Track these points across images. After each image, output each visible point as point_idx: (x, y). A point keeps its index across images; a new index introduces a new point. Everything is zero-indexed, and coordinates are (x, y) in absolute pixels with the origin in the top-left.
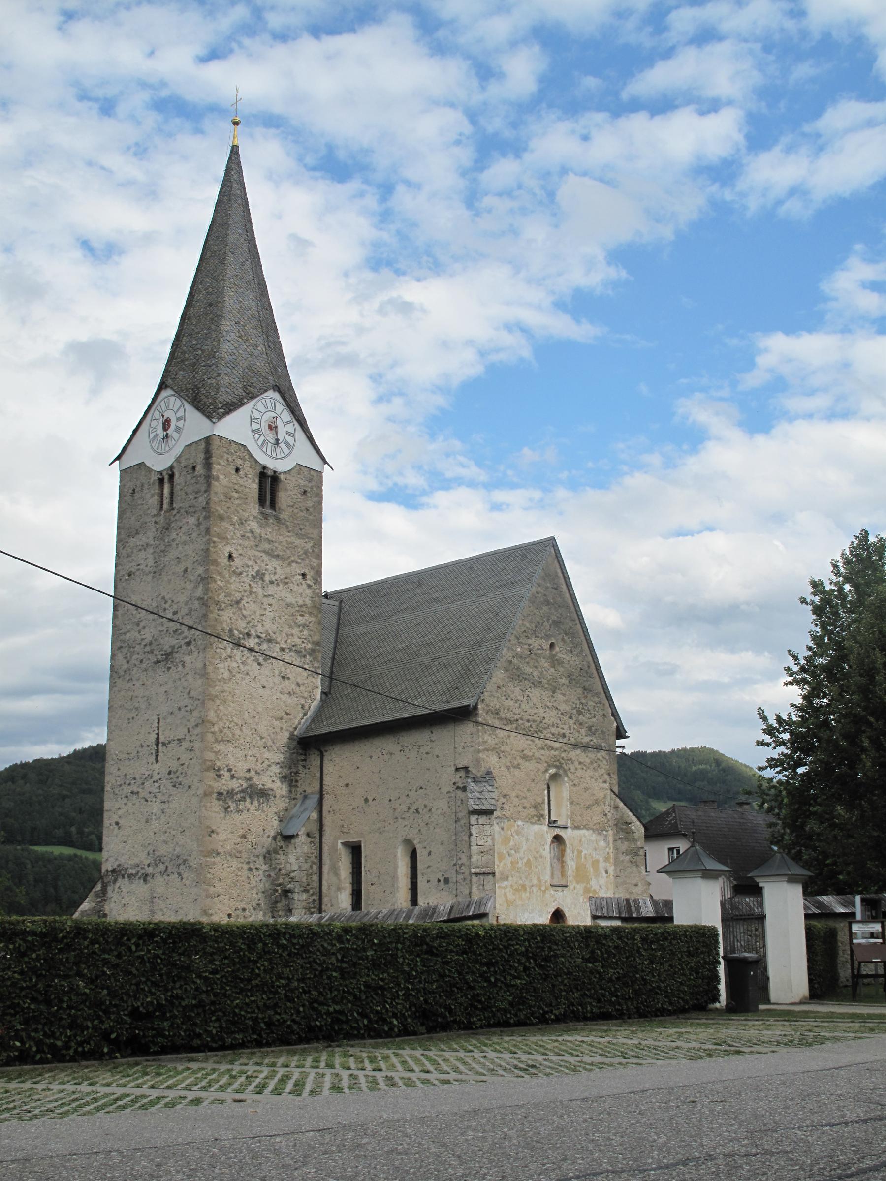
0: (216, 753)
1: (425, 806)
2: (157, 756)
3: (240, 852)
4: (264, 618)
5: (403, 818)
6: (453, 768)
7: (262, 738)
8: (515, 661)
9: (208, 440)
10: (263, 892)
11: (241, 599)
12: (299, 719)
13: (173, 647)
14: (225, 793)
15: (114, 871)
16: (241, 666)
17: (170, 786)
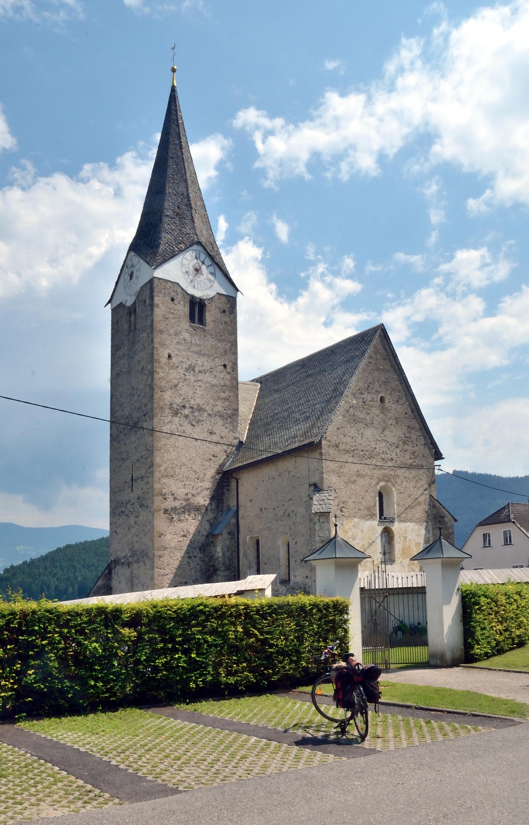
1: (293, 511)
2: (132, 488)
4: (195, 395)
6: (308, 485)
9: (151, 282)
11: (178, 384)
13: (138, 418)
15: (115, 561)
17: (138, 507)
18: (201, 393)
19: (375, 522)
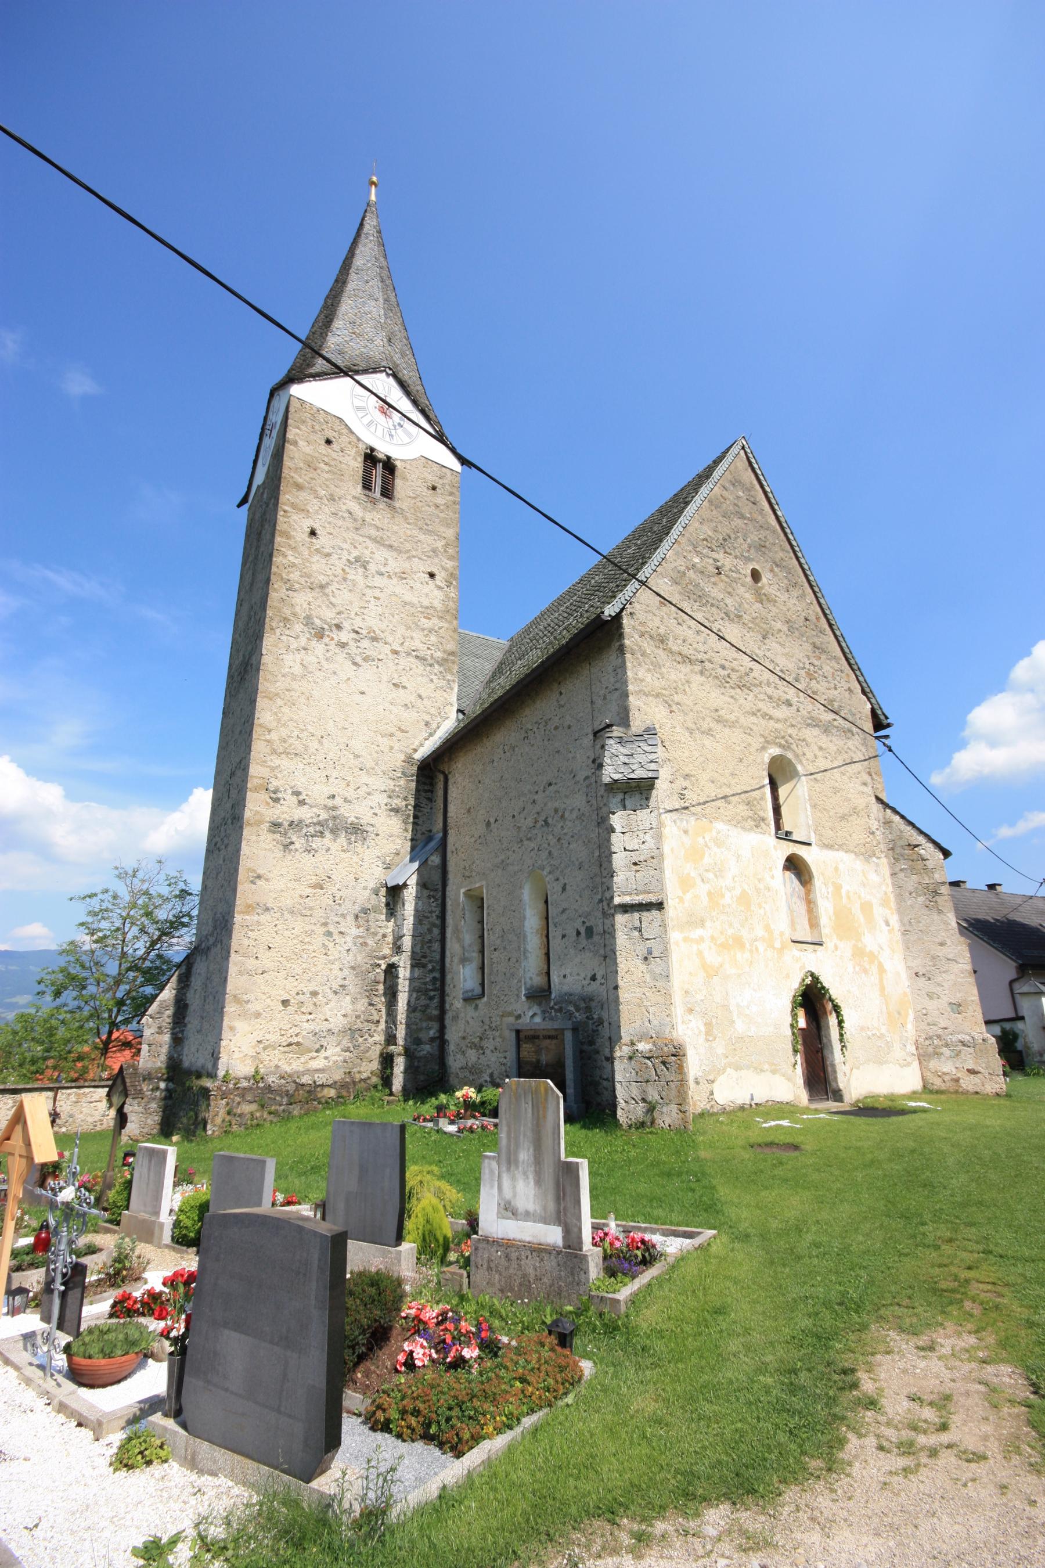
0: (273, 769)
3: (311, 909)
4: (366, 611)
5: (529, 839)
7: (357, 756)
8: (691, 574)
10: (353, 968)
12: (421, 738)
14: (286, 824)
16: (324, 663)
18: (380, 610)
19: (768, 838)
